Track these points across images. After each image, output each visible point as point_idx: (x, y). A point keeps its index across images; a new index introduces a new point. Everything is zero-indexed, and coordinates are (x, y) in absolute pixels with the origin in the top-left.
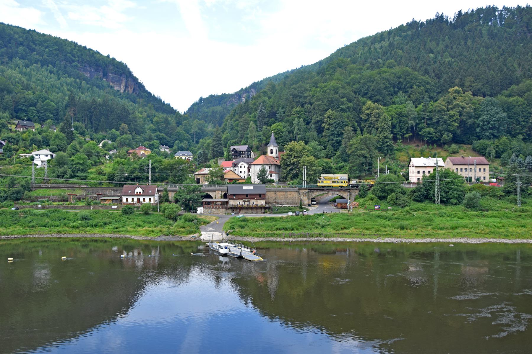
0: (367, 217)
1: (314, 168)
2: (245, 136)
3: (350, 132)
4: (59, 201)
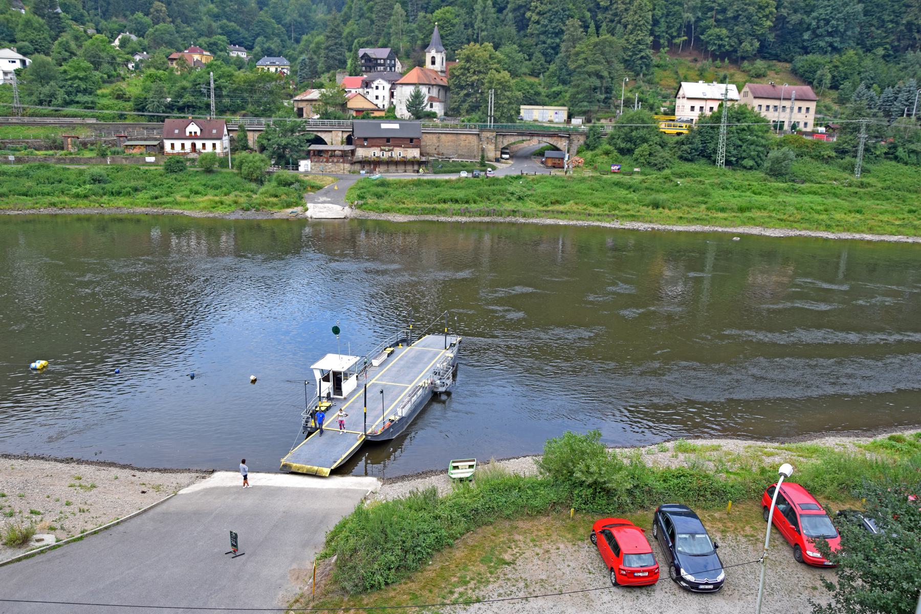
0: (596, 185)
1: (508, 93)
2: (386, 30)
3: (576, 30)
4: (47, 149)
